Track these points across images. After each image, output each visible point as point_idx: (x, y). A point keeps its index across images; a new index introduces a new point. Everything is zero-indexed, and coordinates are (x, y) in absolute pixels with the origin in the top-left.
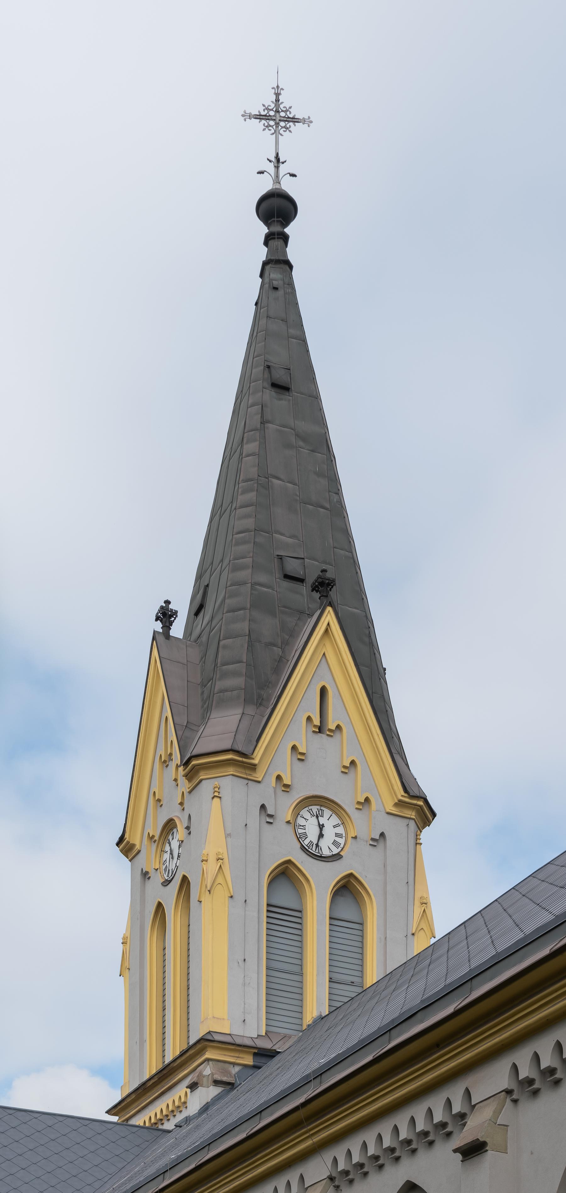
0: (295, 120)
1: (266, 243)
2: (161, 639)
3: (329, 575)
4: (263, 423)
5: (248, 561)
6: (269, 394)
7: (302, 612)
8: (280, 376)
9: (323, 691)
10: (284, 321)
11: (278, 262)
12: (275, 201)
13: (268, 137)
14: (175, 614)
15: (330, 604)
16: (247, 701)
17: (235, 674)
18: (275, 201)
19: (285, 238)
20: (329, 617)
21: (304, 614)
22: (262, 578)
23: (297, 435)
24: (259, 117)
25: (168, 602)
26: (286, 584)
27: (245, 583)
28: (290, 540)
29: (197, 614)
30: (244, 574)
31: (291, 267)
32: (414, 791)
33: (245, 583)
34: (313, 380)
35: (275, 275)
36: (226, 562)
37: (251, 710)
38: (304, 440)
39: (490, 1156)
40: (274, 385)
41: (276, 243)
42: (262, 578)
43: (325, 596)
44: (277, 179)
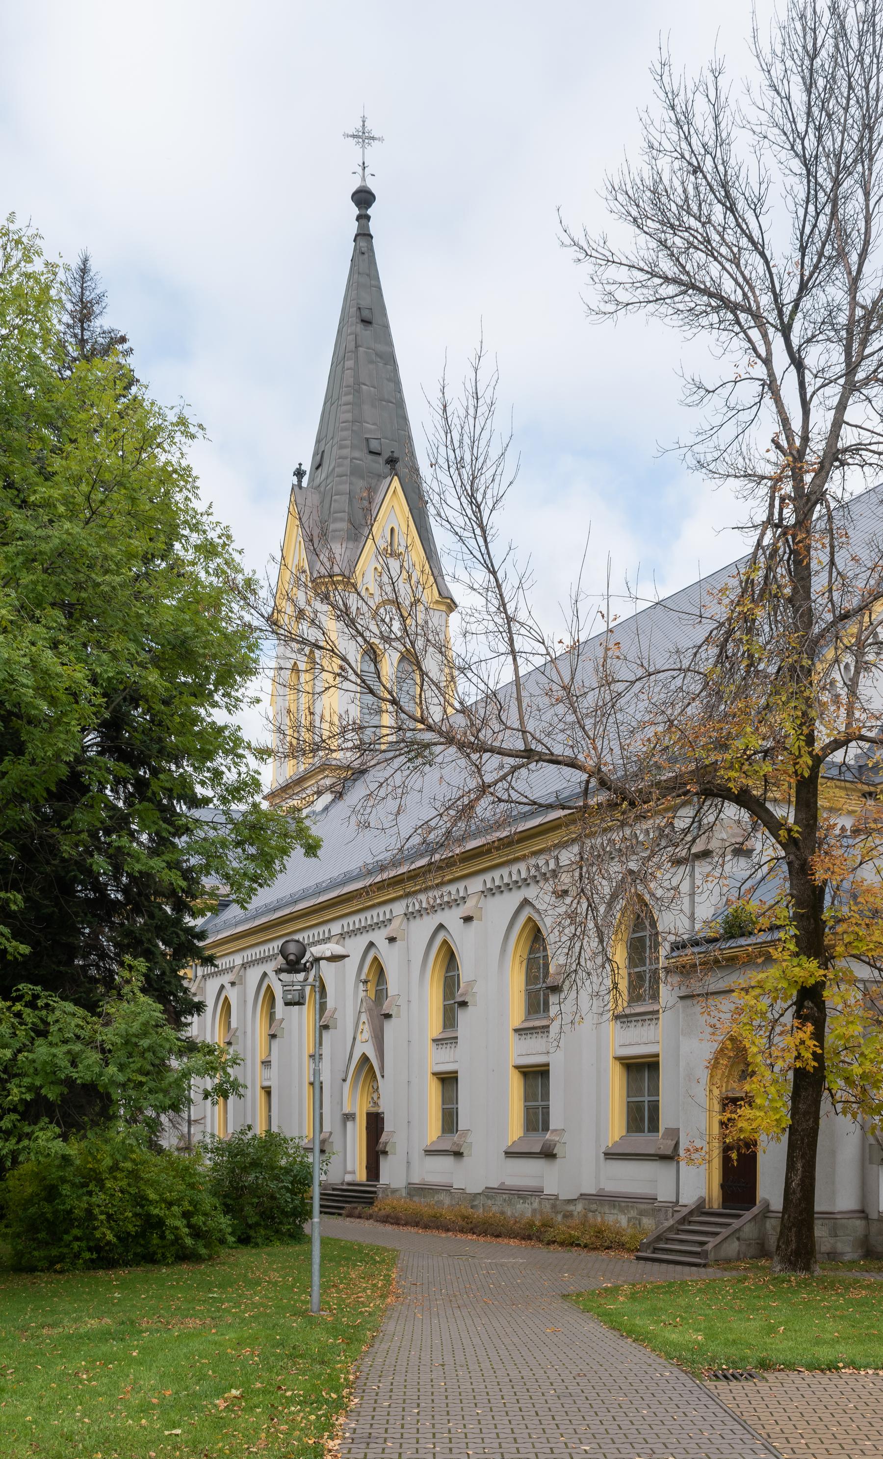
0: (373, 138)
1: (357, 219)
2: (296, 489)
3: (395, 455)
4: (356, 347)
5: (348, 442)
6: (360, 326)
7: (379, 476)
8: (366, 314)
9: (392, 530)
10: (368, 275)
11: (365, 235)
12: (363, 195)
13: (358, 149)
14: (305, 472)
15: (396, 474)
16: (349, 539)
17: (342, 520)
18: (363, 195)
19: (368, 218)
20: (396, 483)
21: (381, 477)
22: (357, 454)
23: (377, 354)
24: (354, 136)
25: (300, 464)
26: (371, 457)
27: (346, 458)
28: (373, 427)
29: (317, 468)
30: (346, 452)
31: (372, 237)
32: (446, 594)
33: (346, 458)
34: (385, 315)
35: (363, 244)
36: (335, 440)
37: (351, 545)
38: (381, 357)
39: (475, 922)
40: (363, 321)
41: (363, 221)
42: (357, 454)
43: (393, 468)
44: (364, 178)
